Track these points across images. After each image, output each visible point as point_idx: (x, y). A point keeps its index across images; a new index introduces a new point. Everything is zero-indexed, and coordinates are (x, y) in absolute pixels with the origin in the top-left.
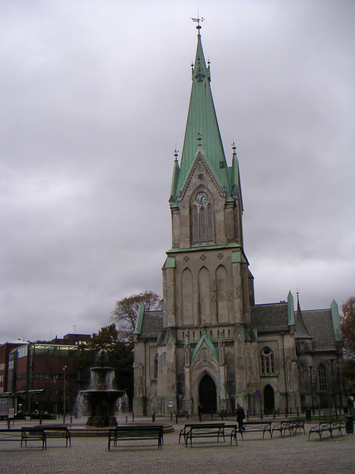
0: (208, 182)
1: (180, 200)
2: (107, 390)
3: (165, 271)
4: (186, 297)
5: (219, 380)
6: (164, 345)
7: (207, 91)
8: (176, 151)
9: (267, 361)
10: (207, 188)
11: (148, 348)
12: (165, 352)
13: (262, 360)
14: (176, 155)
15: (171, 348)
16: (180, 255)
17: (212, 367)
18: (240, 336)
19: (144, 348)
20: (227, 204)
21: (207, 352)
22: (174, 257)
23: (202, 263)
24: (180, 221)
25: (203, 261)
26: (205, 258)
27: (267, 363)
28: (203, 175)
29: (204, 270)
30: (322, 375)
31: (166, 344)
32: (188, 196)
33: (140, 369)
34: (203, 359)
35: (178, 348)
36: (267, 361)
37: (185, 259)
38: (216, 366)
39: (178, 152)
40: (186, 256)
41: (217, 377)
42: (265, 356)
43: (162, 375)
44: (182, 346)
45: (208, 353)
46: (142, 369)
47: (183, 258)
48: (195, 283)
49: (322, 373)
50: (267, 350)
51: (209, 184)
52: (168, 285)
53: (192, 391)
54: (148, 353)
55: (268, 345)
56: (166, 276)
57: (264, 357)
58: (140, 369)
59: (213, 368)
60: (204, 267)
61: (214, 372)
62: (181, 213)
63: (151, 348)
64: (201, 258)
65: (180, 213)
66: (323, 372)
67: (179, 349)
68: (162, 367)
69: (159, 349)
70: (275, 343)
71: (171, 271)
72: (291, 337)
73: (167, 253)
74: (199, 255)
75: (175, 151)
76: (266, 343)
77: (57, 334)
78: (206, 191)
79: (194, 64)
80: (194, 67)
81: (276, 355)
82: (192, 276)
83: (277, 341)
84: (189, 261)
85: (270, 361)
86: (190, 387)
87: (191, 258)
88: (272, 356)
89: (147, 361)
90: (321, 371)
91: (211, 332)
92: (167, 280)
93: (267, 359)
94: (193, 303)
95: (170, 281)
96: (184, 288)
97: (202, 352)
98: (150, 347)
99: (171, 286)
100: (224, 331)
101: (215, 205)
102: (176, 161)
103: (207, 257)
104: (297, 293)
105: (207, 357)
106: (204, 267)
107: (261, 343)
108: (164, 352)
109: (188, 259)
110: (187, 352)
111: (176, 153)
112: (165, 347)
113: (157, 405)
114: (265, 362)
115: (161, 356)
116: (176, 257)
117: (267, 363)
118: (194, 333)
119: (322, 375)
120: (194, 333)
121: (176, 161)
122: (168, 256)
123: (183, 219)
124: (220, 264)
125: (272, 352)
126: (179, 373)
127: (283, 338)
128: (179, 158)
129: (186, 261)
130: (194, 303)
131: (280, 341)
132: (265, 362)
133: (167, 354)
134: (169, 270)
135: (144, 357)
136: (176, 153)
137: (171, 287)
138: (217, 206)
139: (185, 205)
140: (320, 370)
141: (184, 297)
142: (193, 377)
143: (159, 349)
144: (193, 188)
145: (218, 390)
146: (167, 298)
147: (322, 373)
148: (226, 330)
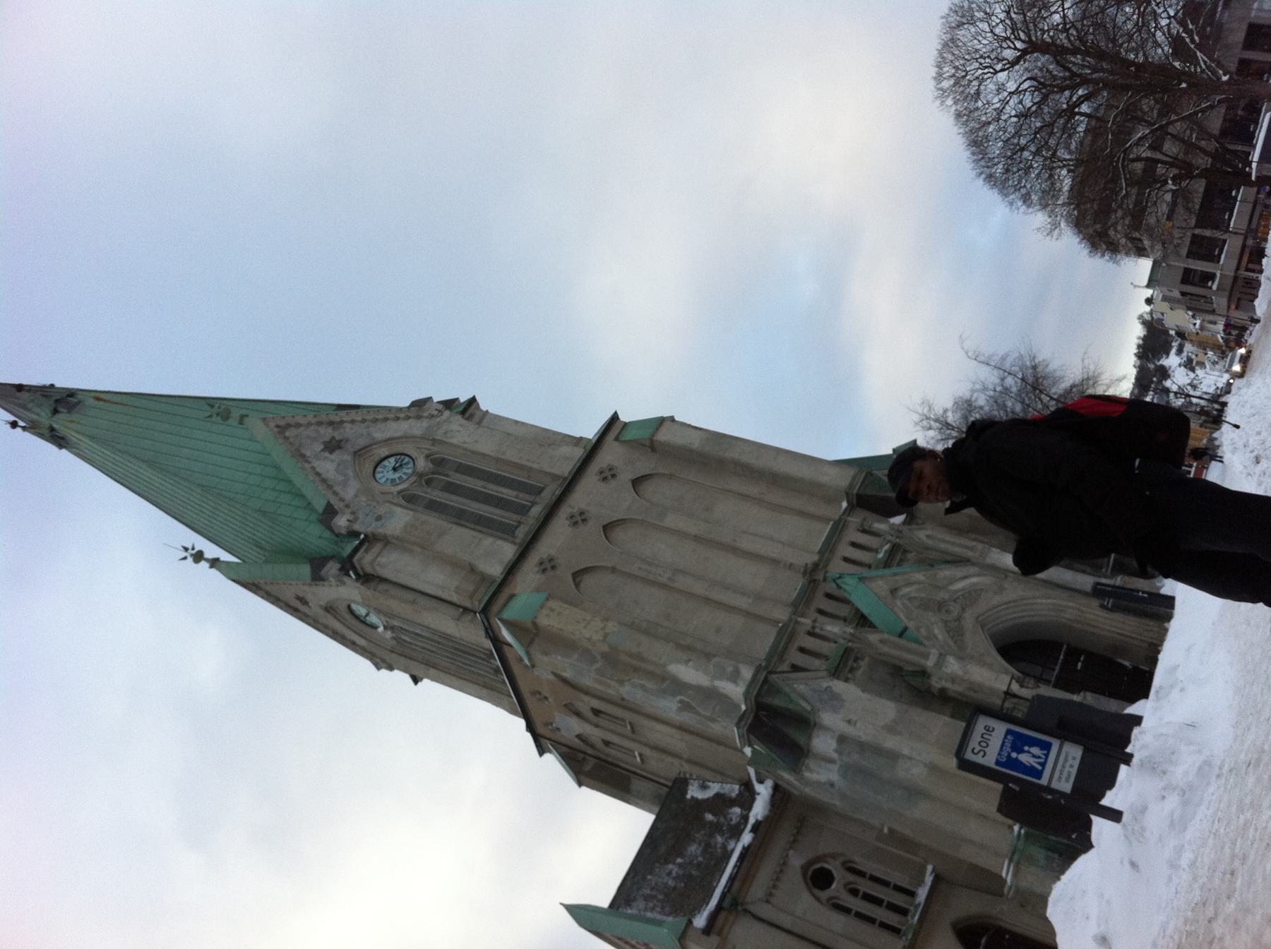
1: (351, 518)
7: (116, 399)
9: (892, 884)
10: (380, 442)
19: (758, 927)
34: (930, 614)
36: (892, 884)
47: (538, 572)
48: (640, 569)
63: (772, 900)
71: (552, 610)
77: (558, 903)
79: (12, 418)
80: (21, 423)
84: (550, 573)
87: (553, 552)
95: (585, 627)
97: (903, 604)
98: (767, 902)
101: (448, 440)
102: (214, 563)
109: (553, 568)
121: (214, 563)
128: (211, 551)
137: (607, 631)
143: (811, 771)
148: (845, 550)
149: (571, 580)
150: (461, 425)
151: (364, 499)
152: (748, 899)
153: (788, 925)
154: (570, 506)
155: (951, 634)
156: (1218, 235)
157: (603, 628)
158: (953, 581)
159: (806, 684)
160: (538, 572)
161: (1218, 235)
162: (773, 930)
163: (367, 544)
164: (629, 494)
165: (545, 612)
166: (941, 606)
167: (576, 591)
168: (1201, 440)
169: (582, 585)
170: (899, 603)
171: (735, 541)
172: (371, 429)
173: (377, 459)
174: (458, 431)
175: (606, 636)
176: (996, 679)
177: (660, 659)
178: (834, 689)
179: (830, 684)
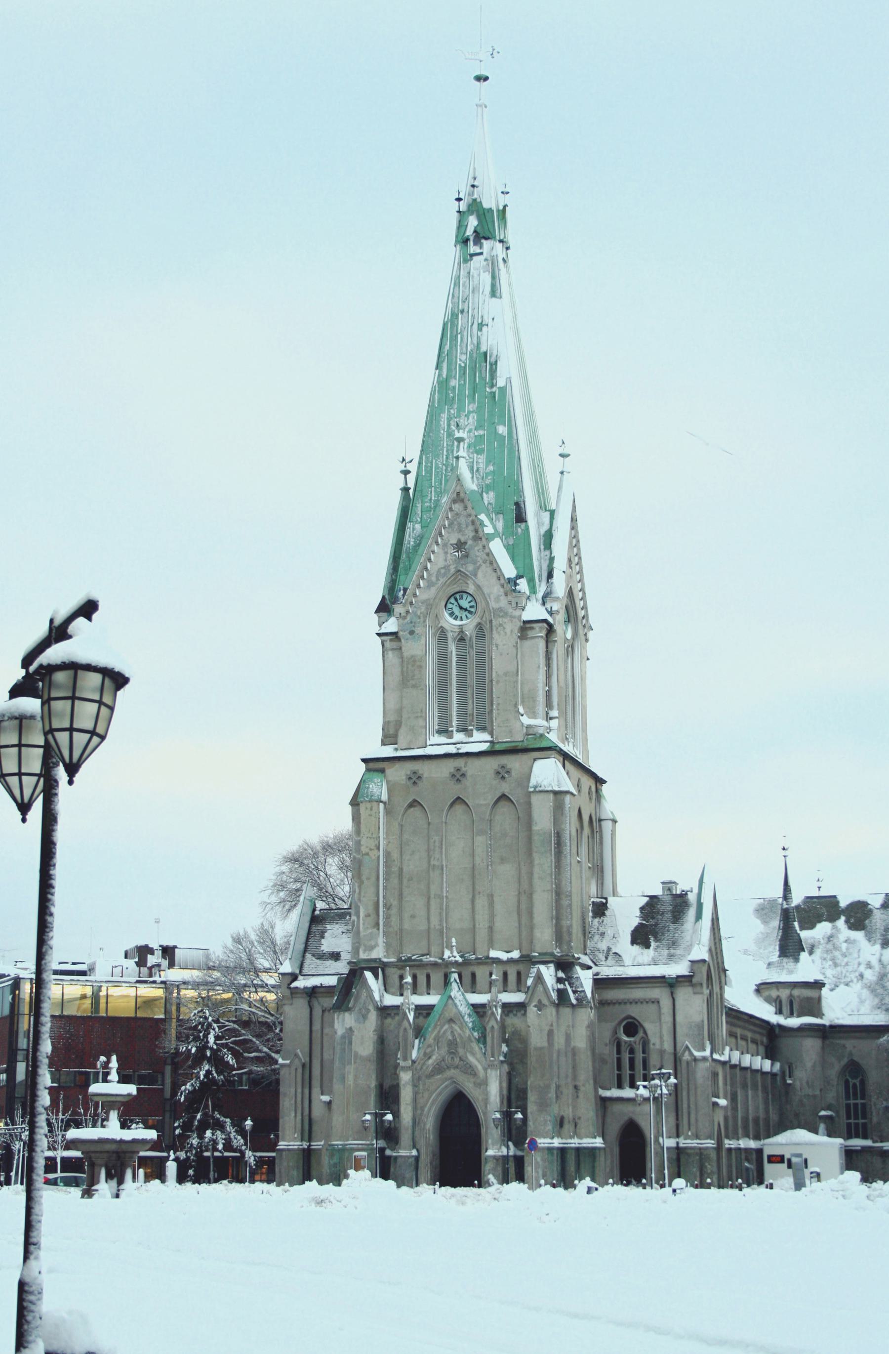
0: (479, 564)
2: (751, 1089)
3: (356, 807)
4: (410, 879)
5: (486, 1107)
6: (348, 1009)
8: (404, 460)
11: (317, 1011)
12: (351, 1029)
13: (619, 1052)
14: (406, 473)
15: (365, 1017)
16: (398, 765)
17: (470, 1070)
18: (541, 989)
20: (528, 626)
21: (458, 1029)
22: (382, 771)
23: (455, 790)
24: (402, 672)
25: (459, 786)
26: (463, 775)
27: (632, 1061)
28: (465, 543)
29: (459, 808)
30: (855, 1095)
31: (354, 1006)
32: (422, 603)
33: (296, 1069)
34: (446, 1049)
35: (386, 1018)
37: (410, 778)
38: (480, 1067)
39: (411, 461)
40: (413, 769)
41: (480, 1098)
42: (626, 1042)
43: (344, 1088)
44: (395, 1011)
45: (461, 1032)
46: (300, 1070)
48: (435, 842)
49: (855, 1085)
50: (632, 1027)
51: (480, 570)
52: (364, 849)
53: (417, 1133)
54: (317, 1026)
55: (634, 1011)
56: (360, 823)
57: (623, 1044)
58: (296, 1069)
59: (471, 1074)
60: (459, 798)
61: (474, 1083)
62: (403, 649)
63: (326, 1014)
64: (453, 776)
65: (400, 648)
66: (858, 1084)
67: (388, 1021)
68: (345, 1068)
69: (338, 1018)
70: (653, 1007)
71: (371, 809)
72: (695, 993)
73: (364, 760)
74: (449, 766)
75: (401, 460)
76: (628, 1006)
78: (471, 589)
81: (654, 1039)
82: (429, 824)
83: (658, 1002)
84: (420, 783)
85: (639, 1056)
86: (411, 1124)
87: (425, 775)
88: (645, 1043)
89: (314, 1047)
90: (852, 1082)
91: (473, 975)
92: (362, 835)
93: (632, 1051)
94: (429, 899)
96: (406, 857)
97: (446, 1030)
98: (323, 1011)
99: (371, 850)
100: (505, 975)
103: (469, 774)
104: (784, 849)
105: (456, 1044)
106: (459, 798)
107: (617, 1006)
108: (348, 1027)
110: (405, 1029)
111: (405, 467)
112: (351, 1014)
113: (330, 1169)
114: (626, 1057)
115: (343, 1037)
116: (389, 772)
117: (632, 1061)
118: (428, 977)
119: (855, 1095)
120: (428, 977)
122: (368, 770)
123: (410, 667)
124: (500, 795)
125: (645, 1032)
126: (387, 1084)
127: (672, 993)
129: (415, 783)
130: (432, 896)
131: (666, 1003)
132: (626, 1057)
133: (356, 1033)
134: (366, 808)
135: (307, 1037)
136: (405, 467)
138: (498, 633)
139: (414, 626)
140: (850, 1080)
141: (405, 881)
142: (420, 1095)
144: (438, 580)
145: (483, 1131)
146: (361, 883)
147: (855, 1085)
149: (411, 800)
150: (512, 631)
151: (422, 610)
152: (320, 999)
153: (314, 1028)
154: (466, 763)
155: (437, 1066)
156: (59, 1160)
157: (371, 850)
158: (473, 1054)
159: (367, 997)
160: (407, 775)
161: (59, 1160)
162: (309, 1022)
163: (394, 637)
164: (491, 799)
165: (369, 805)
166: (453, 1052)
167: (403, 810)
168: (747, 1169)
169: (412, 809)
170: (446, 1026)
171: (479, 893)
172: (484, 565)
173: (464, 589)
174: (506, 633)
175: (367, 854)
176: (407, 1104)
177: (364, 897)
178: (370, 1014)
179: (372, 1010)
